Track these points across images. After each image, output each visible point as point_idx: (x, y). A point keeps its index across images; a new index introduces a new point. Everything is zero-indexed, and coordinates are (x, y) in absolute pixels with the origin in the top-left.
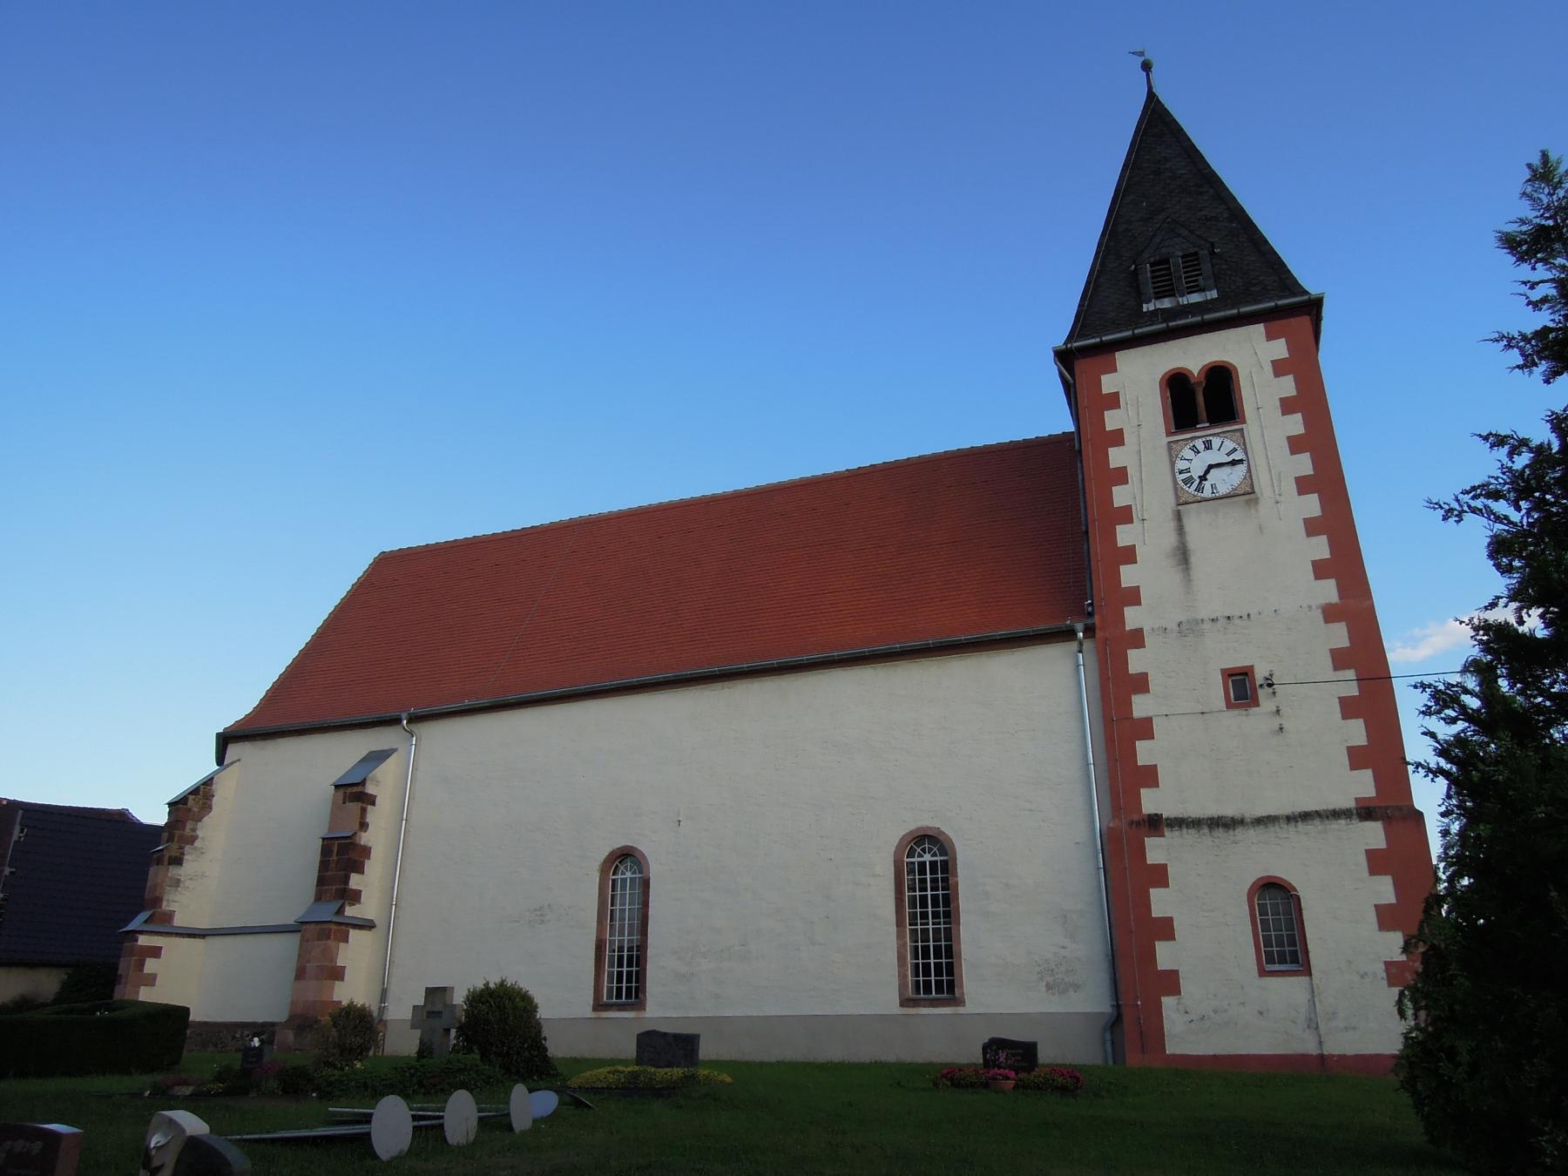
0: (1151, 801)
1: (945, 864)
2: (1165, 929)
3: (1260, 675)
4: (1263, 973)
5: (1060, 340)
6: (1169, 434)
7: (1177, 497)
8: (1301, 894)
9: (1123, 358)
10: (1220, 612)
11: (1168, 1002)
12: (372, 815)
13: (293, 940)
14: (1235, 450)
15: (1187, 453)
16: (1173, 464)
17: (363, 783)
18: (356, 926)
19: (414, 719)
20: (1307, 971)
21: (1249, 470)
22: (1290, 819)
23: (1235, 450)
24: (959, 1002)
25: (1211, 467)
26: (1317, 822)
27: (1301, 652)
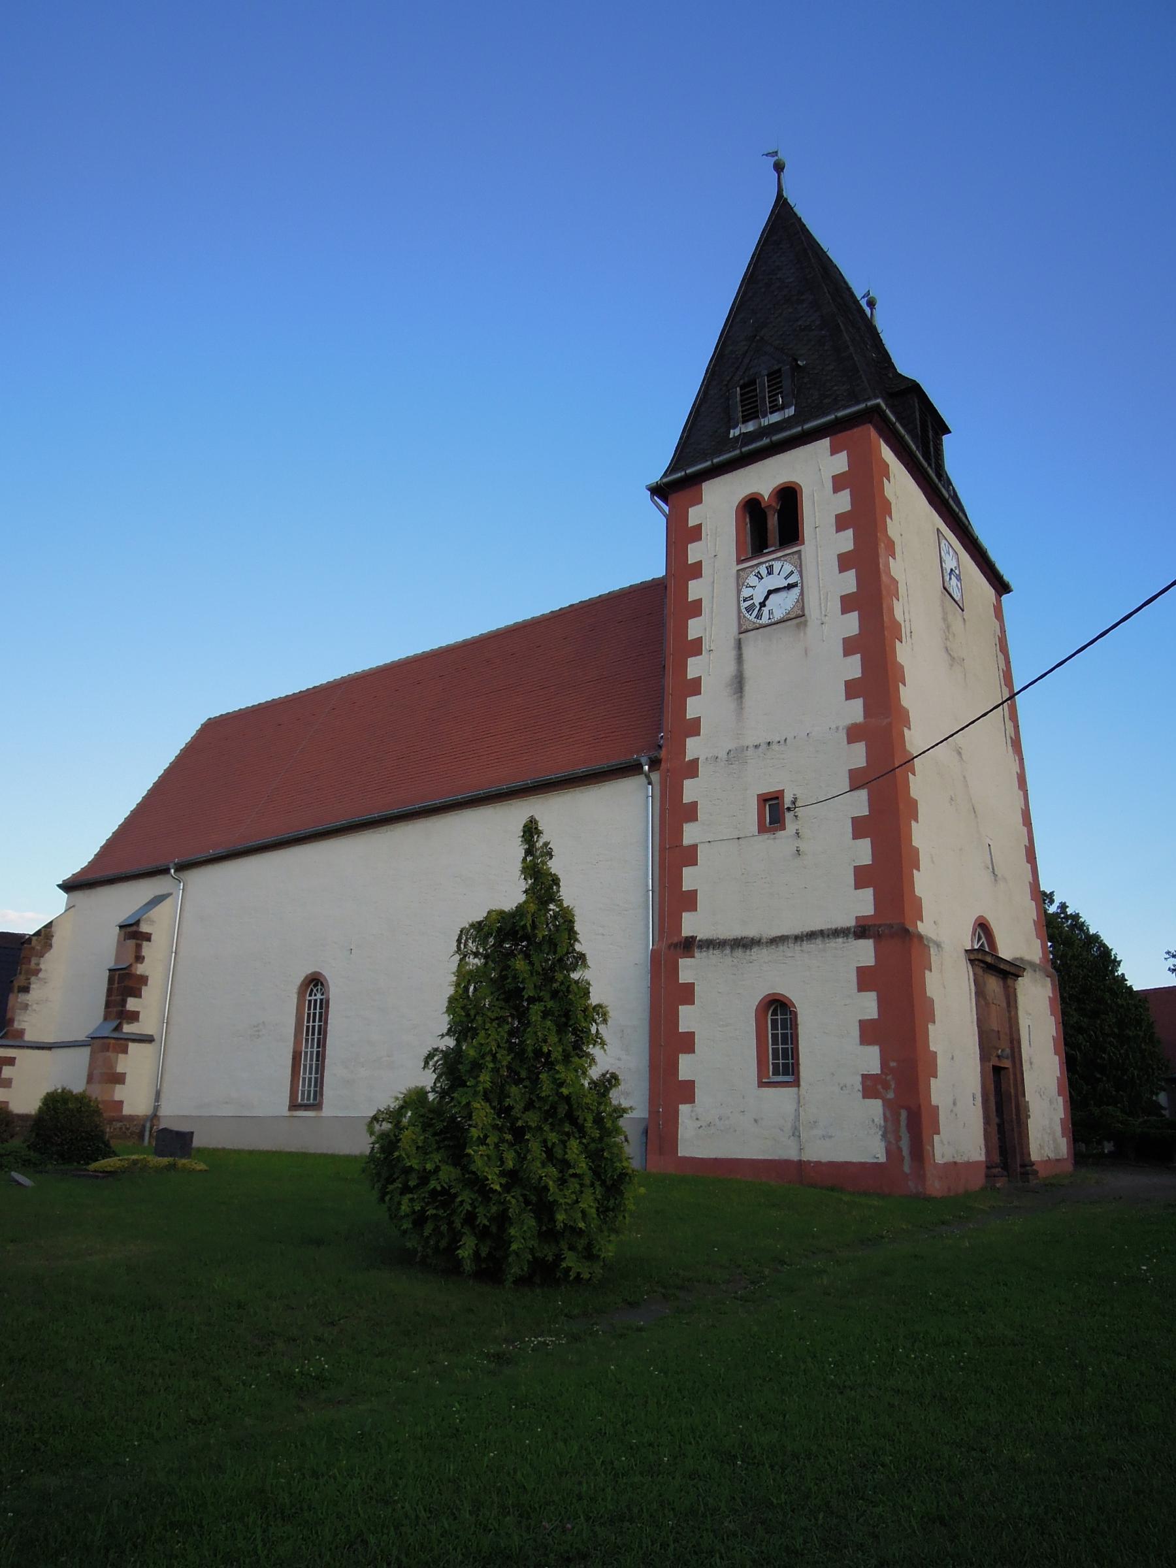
0: (691, 925)
4: (761, 1084)
5: (656, 472)
7: (740, 625)
8: (799, 1011)
10: (762, 739)
11: (684, 1109)
12: (147, 949)
13: (86, 1051)
15: (752, 580)
16: (739, 592)
17: (137, 923)
18: (134, 1041)
19: (182, 867)
20: (796, 1083)
21: (802, 593)
22: (798, 938)
23: (792, 573)
25: (770, 592)
26: (819, 941)
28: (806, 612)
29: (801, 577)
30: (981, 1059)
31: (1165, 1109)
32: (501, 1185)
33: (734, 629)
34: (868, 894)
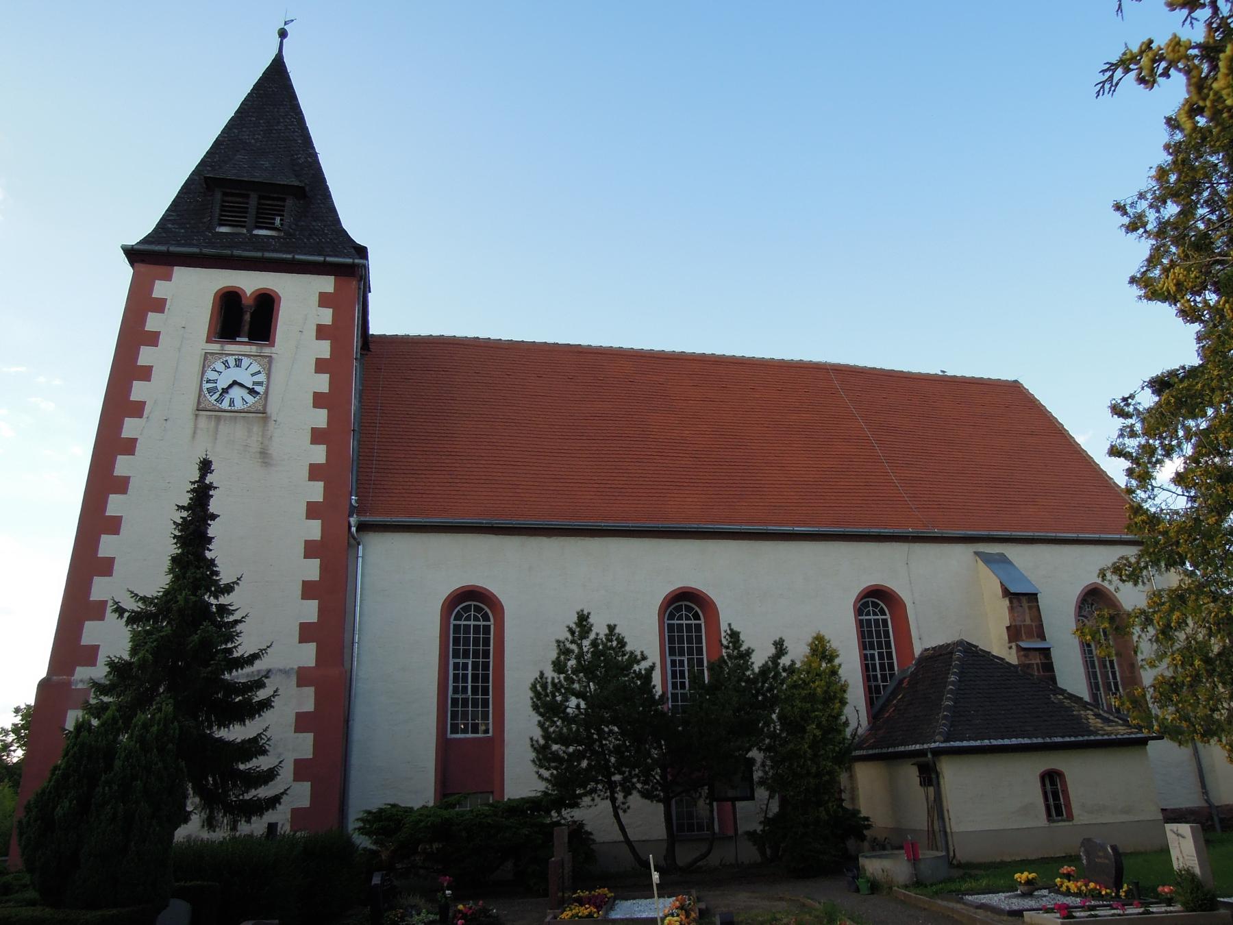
1: (865, 648)
6: (209, 341)
7: (199, 403)
9: (179, 272)
14: (259, 372)
15: (219, 366)
23: (259, 372)
29: (269, 376)
31: (607, 913)
34: (319, 486)
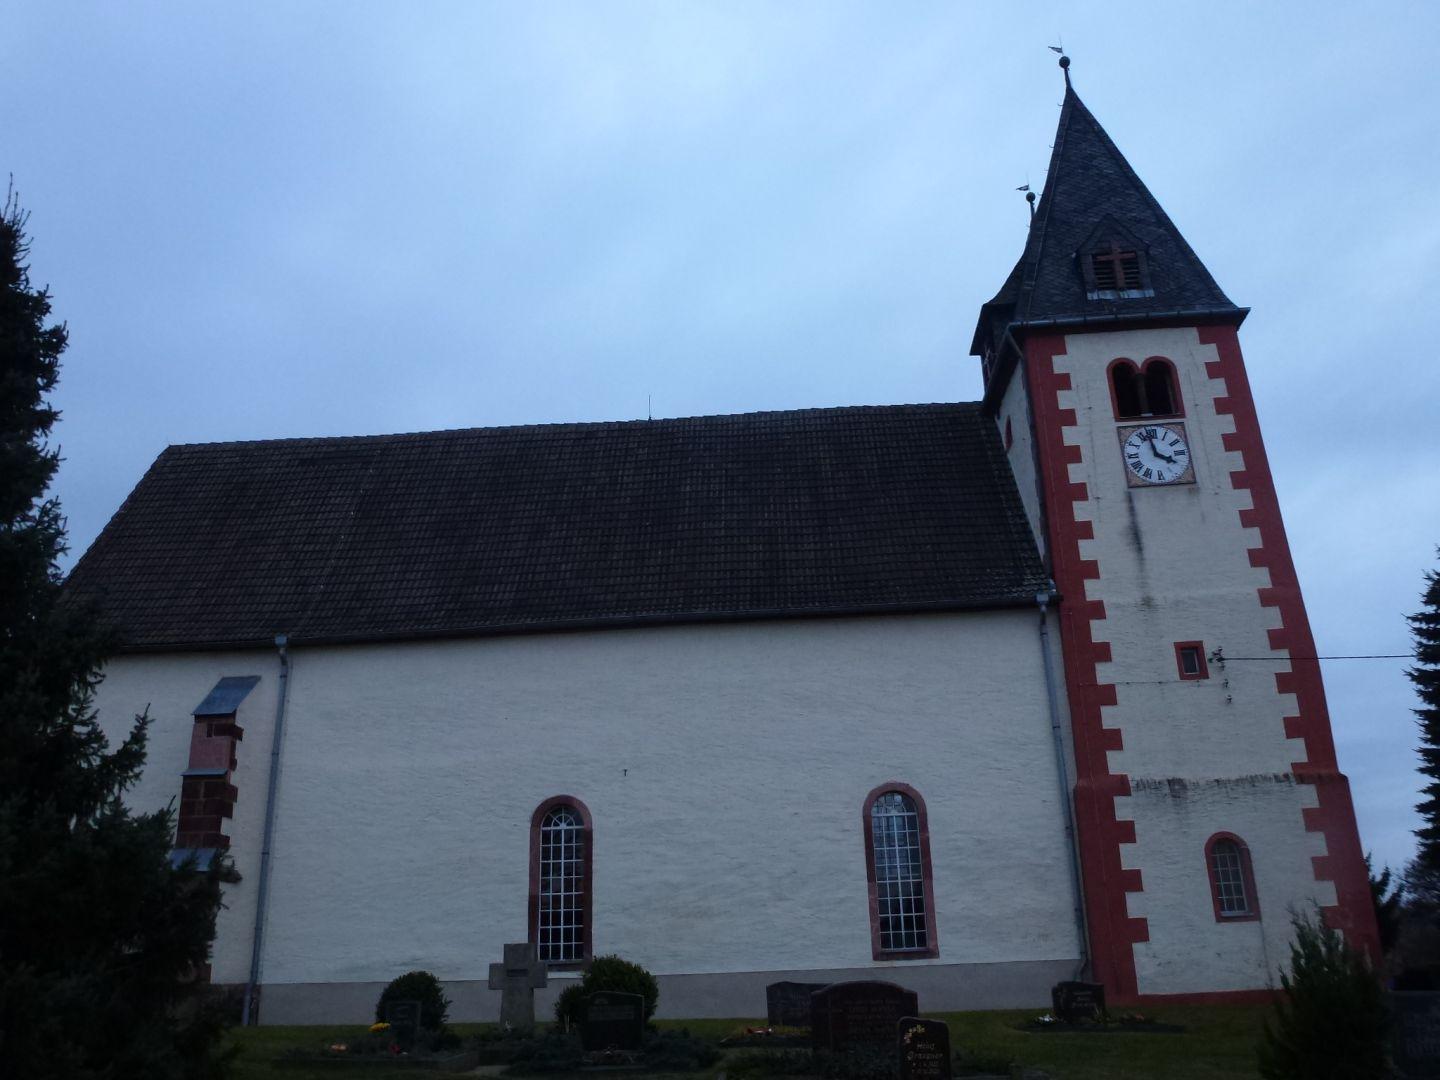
2: (1134, 881)
3: (1209, 650)
4: (1220, 919)
7: (1129, 481)
8: (1250, 848)
15: (1136, 440)
16: (1122, 449)
17: (233, 715)
24: (932, 953)
25: (1157, 455)
27: (1241, 630)
28: (1198, 479)
29: (1187, 445)
30: (926, 814)
32: (172, 862)
33: (1123, 483)
